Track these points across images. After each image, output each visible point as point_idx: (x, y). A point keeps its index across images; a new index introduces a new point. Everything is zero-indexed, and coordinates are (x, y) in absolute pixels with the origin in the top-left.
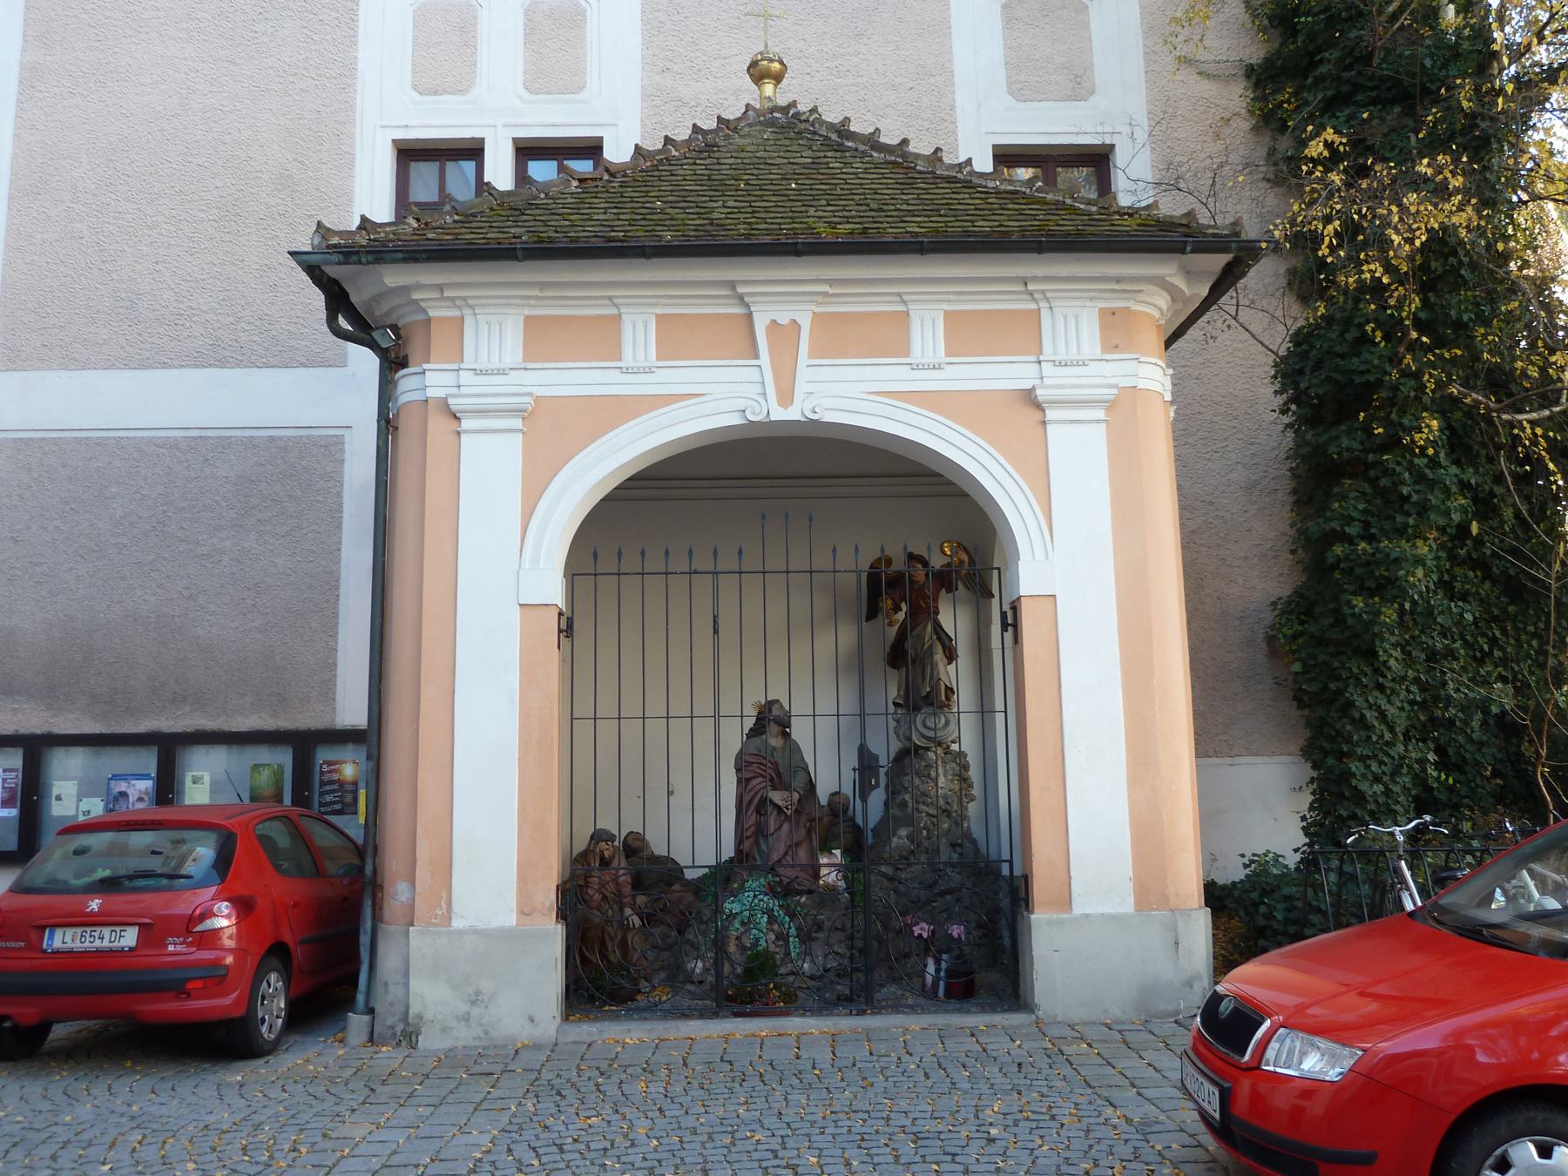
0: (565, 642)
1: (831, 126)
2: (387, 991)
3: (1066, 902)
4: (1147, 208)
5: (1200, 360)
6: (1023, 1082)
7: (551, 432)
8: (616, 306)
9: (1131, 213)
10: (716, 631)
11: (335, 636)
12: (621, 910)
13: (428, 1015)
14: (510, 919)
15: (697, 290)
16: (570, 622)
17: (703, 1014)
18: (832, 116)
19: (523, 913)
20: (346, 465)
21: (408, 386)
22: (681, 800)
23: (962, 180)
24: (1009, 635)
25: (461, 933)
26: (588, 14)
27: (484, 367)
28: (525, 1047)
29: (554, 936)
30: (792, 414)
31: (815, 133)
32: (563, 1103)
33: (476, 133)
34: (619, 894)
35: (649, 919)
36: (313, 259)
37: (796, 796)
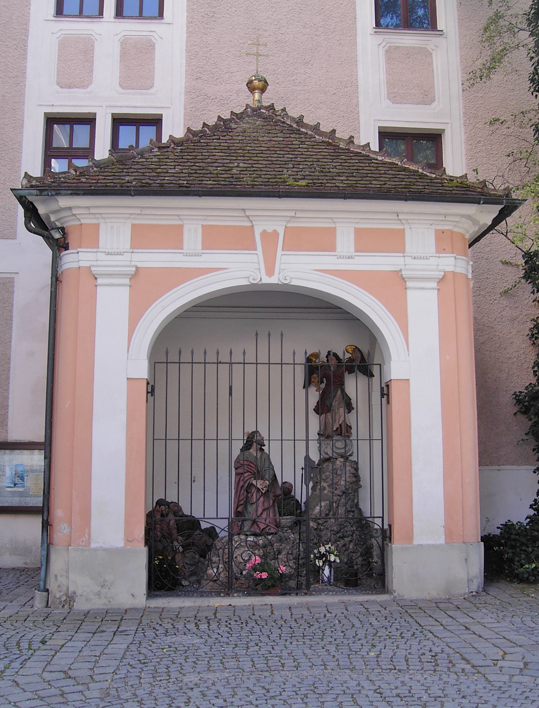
0: (151, 398)
1: (293, 119)
2: (56, 580)
3: (409, 537)
4: (461, 177)
5: (489, 249)
6: (388, 624)
7: (144, 286)
8: (181, 219)
9: (452, 179)
10: (231, 394)
11: (7, 390)
12: (172, 542)
13: (79, 592)
14: (121, 544)
15: (226, 211)
16: (153, 388)
17: (218, 594)
18: (294, 113)
19: (128, 540)
20: (15, 295)
21: (70, 260)
22: (198, 485)
23: (363, 156)
24: (384, 400)
25: (96, 550)
26: (156, 46)
27: (110, 251)
28: (131, 609)
29: (142, 552)
30: (274, 280)
31: (284, 123)
32: (157, 632)
33: (92, 110)
34: (171, 535)
35: (186, 547)
36: (22, 193)
37: (267, 482)
